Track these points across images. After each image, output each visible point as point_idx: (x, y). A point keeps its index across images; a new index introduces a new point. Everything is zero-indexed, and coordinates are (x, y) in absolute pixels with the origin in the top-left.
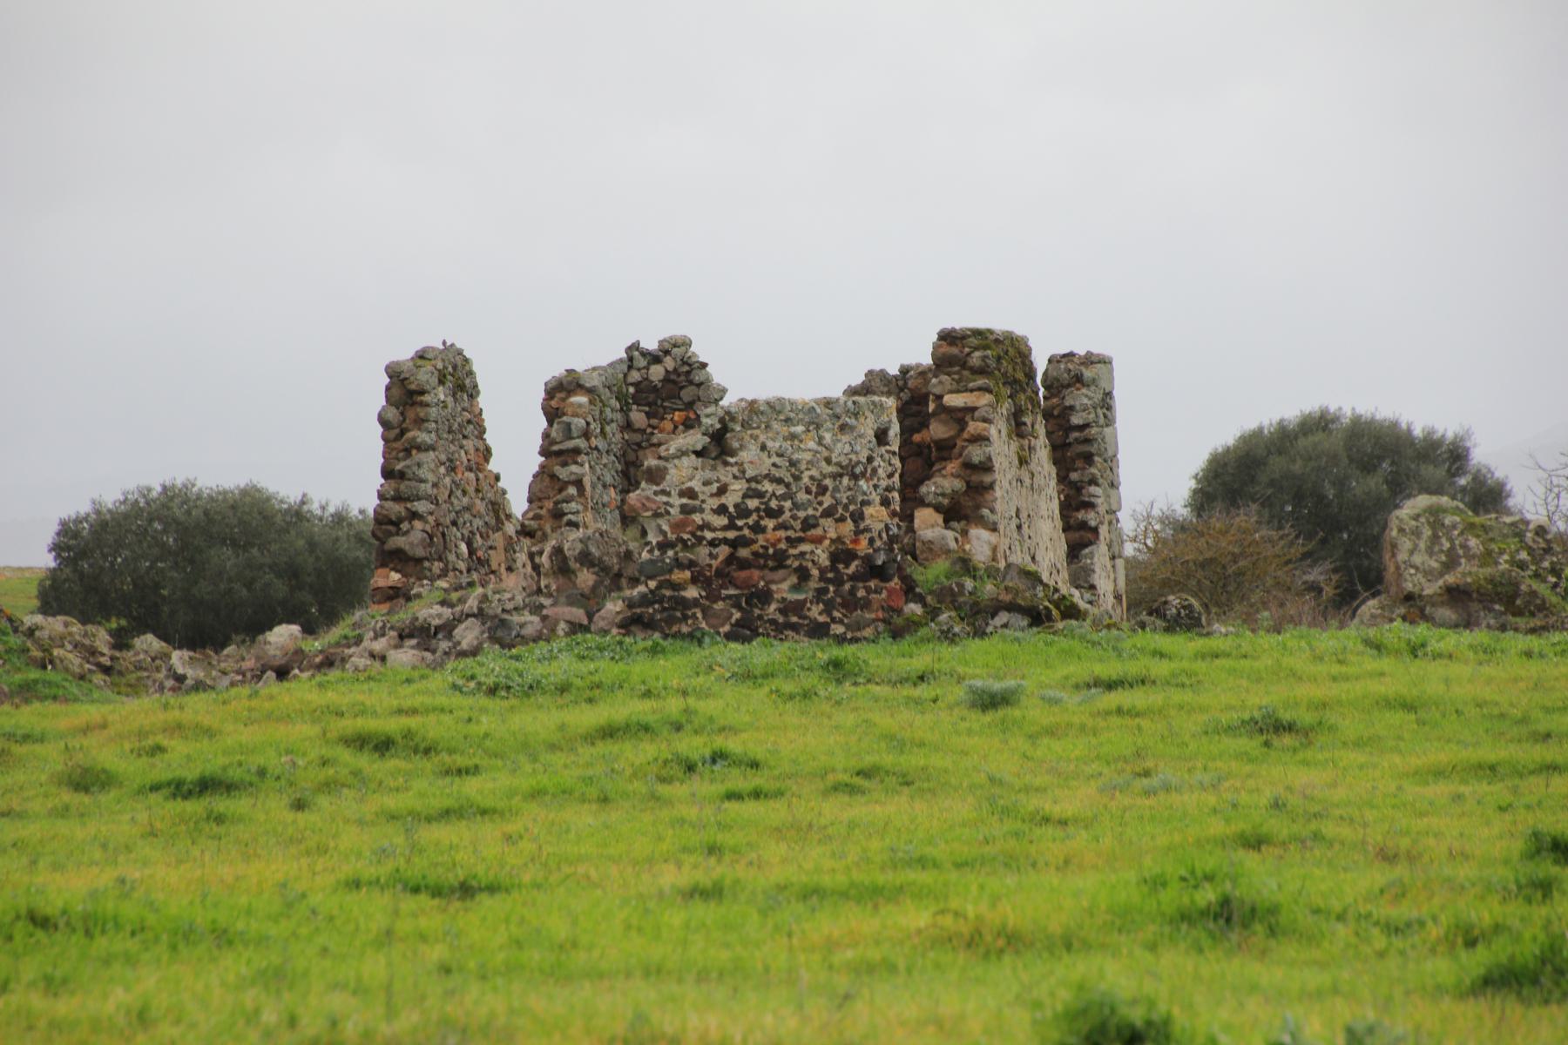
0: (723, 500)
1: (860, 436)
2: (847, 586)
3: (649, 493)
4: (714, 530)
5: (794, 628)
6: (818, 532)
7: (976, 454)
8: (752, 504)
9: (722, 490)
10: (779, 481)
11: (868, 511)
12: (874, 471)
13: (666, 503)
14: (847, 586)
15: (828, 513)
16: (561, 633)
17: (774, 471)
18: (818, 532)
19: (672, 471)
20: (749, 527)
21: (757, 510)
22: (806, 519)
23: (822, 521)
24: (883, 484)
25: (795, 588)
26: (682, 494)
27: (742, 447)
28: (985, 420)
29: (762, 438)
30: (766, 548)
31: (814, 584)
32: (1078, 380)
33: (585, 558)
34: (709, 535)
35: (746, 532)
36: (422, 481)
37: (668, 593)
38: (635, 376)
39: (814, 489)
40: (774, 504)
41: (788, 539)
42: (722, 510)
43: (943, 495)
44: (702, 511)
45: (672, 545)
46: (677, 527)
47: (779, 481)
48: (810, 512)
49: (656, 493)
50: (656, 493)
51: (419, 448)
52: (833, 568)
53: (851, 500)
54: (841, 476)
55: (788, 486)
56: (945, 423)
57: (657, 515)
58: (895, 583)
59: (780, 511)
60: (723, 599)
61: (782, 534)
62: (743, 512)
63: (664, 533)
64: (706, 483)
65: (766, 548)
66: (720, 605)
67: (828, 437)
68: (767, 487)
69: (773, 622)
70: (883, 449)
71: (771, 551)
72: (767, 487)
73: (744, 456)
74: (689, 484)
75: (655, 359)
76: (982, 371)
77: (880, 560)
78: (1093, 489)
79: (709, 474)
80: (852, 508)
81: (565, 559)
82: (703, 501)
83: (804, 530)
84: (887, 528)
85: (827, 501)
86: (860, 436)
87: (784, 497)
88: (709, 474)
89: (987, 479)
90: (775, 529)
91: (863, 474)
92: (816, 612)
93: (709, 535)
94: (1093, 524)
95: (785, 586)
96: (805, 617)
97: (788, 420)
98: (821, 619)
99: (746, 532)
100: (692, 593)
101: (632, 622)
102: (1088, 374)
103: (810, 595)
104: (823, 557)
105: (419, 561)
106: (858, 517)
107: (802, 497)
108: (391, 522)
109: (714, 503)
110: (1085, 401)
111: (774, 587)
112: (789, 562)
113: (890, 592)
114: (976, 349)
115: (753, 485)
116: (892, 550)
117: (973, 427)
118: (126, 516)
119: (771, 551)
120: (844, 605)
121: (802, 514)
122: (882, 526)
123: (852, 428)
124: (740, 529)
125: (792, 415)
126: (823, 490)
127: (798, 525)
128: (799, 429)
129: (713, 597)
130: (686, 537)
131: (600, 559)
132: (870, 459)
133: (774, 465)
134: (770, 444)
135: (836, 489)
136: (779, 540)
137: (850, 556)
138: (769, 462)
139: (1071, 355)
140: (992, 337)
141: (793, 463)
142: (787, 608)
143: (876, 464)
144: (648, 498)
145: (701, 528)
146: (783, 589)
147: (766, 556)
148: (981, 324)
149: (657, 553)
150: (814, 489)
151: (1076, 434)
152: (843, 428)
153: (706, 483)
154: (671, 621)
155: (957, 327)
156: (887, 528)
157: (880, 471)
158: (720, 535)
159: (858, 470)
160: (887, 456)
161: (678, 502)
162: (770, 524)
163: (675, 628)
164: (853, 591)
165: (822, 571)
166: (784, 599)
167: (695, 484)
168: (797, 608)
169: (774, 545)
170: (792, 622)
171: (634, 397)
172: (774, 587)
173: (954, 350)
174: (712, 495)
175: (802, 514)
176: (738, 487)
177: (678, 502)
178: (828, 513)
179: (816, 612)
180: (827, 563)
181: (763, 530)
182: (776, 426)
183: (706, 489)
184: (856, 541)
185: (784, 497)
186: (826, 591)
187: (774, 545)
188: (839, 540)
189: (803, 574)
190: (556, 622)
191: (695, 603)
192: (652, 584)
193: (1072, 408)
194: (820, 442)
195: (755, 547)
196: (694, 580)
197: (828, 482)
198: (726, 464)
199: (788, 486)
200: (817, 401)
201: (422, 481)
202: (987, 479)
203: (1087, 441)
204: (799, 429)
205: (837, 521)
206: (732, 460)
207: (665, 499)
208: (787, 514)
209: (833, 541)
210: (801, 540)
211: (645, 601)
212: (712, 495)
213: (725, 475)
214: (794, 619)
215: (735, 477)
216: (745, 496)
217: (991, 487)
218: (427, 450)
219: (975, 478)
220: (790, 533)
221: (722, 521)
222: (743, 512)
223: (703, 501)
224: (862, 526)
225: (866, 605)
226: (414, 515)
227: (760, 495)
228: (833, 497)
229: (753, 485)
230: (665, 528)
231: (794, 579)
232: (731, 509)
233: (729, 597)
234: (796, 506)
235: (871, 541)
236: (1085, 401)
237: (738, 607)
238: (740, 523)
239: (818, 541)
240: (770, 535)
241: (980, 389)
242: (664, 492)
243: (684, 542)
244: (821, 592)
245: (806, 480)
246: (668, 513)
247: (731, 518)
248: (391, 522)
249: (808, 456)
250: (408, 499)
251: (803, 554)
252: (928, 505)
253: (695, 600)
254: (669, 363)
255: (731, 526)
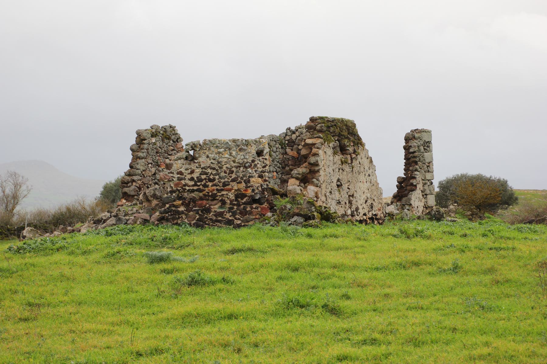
0: (193, 175)
1: (249, 153)
2: (242, 207)
3: (167, 173)
4: (189, 186)
5: (219, 221)
6: (230, 187)
7: (312, 160)
8: (203, 177)
9: (192, 172)
10: (214, 169)
11: (252, 180)
12: (256, 165)
13: (172, 177)
14: (242, 207)
15: (233, 180)
16: (138, 223)
17: (212, 165)
18: (230, 187)
19: (175, 165)
20: (202, 185)
21: (205, 179)
22: (224, 182)
23: (231, 183)
24: (260, 170)
25: (221, 207)
26: (178, 173)
27: (199, 157)
28: (318, 148)
29: (207, 153)
30: (208, 193)
31: (228, 206)
32: (414, 138)
33: (155, 196)
34: (187, 188)
35: (201, 187)
36: (138, 169)
37: (174, 209)
38: (288, 138)
39: (228, 172)
40: (212, 177)
41: (217, 190)
42: (192, 179)
43: (299, 174)
44: (185, 179)
45: (174, 192)
46: (176, 185)
47: (214, 169)
48: (226, 180)
49: (169, 173)
50: (169, 173)
51: (139, 158)
52: (236, 200)
53: (244, 176)
54: (240, 167)
55: (217, 170)
56: (306, 149)
57: (169, 181)
58: (266, 205)
59: (214, 180)
60: (193, 211)
61: (215, 188)
62: (200, 180)
63: (172, 187)
64: (187, 169)
65: (208, 193)
66: (191, 213)
67: (234, 153)
68: (209, 171)
69: (211, 219)
70: (261, 158)
71: (210, 194)
72: (209, 171)
73: (200, 159)
74: (180, 170)
75: (294, 133)
76: (320, 131)
77: (257, 197)
78: (416, 173)
79: (187, 166)
80: (244, 178)
81: (147, 197)
82: (185, 176)
83: (223, 186)
84: (261, 186)
85: (234, 176)
86: (249, 153)
87: (215, 175)
88: (187, 166)
89: (317, 168)
90: (212, 186)
91: (250, 166)
92: (228, 216)
93: (187, 188)
94: (415, 184)
95: (217, 206)
96: (224, 218)
97: (217, 147)
98: (230, 218)
99: (201, 187)
100: (182, 209)
101: (161, 220)
102: (417, 135)
103: (227, 210)
104: (232, 196)
105: (133, 196)
106: (247, 182)
107: (223, 174)
108: (125, 183)
109: (189, 176)
110: (415, 144)
111: (212, 207)
112: (217, 198)
113: (262, 209)
114: (320, 123)
115: (204, 170)
116: (264, 194)
117: (314, 150)
118: (452, 180)
119: (210, 194)
120: (241, 213)
121: (223, 181)
122: (260, 185)
123: (245, 150)
124: (199, 186)
125: (219, 145)
126: (232, 172)
127: (221, 185)
128: (222, 150)
129: (189, 210)
130: (179, 189)
131: (160, 197)
132: (253, 161)
133: (211, 163)
134: (210, 155)
135: (237, 172)
136: (214, 190)
137: (243, 196)
138: (210, 162)
139: (417, 130)
140: (326, 119)
141: (219, 163)
142: (218, 214)
143: (256, 163)
144: (166, 175)
145: (185, 185)
146: (216, 207)
147: (209, 196)
148: (321, 115)
149: (169, 194)
150: (228, 172)
151: (411, 155)
152: (241, 150)
153: (187, 169)
154: (174, 219)
155: (315, 116)
156: (261, 186)
157: (258, 165)
158: (191, 188)
159: (247, 165)
160: (262, 160)
161: (176, 176)
162: (210, 184)
163: (175, 222)
164: (245, 208)
165: (231, 201)
166: (215, 211)
167: (183, 170)
168: (221, 214)
169: (211, 192)
170: (219, 221)
171: (287, 144)
172: (212, 207)
173: (312, 124)
174: (189, 174)
175: (223, 181)
176: (198, 171)
177: (176, 176)
178: (233, 180)
179: (228, 216)
180: (234, 198)
181: (208, 186)
182: (212, 149)
183: (186, 171)
184: (246, 190)
185: (215, 175)
186: (233, 208)
187: (211, 192)
188: (239, 190)
189: (223, 203)
190: (138, 218)
191: (182, 212)
192: (167, 206)
193: (411, 146)
194: (231, 154)
195: (204, 192)
196: (182, 204)
197: (234, 169)
198: (194, 162)
199: (217, 170)
200: (230, 141)
201: (138, 169)
202: (317, 168)
203: (415, 157)
204: (222, 150)
205: (238, 183)
206: (196, 161)
207: (172, 175)
208: (217, 181)
209: (236, 190)
210: (222, 190)
211: (166, 212)
212: (189, 174)
213: (193, 166)
214: (220, 218)
215: (197, 167)
216: (201, 174)
217: (318, 171)
218: (142, 159)
219: (313, 168)
220: (218, 187)
221: (192, 183)
222: (200, 180)
223: (185, 176)
224: (249, 185)
225: (251, 213)
226: (133, 181)
227: (206, 174)
228: (236, 175)
229: (204, 170)
230: (172, 185)
231: (220, 204)
232: (195, 179)
233: (195, 210)
234: (220, 178)
235: (253, 191)
236: (415, 144)
237: (198, 213)
238: (199, 184)
239: (230, 190)
240: (210, 188)
241: (317, 137)
242: (171, 173)
243: (179, 190)
244: (230, 209)
245: (224, 168)
246: (173, 180)
247: (196, 182)
248: (125, 183)
249: (225, 160)
250: (133, 175)
251: (223, 195)
252: (293, 178)
253: (182, 211)
254: (297, 134)
255: (195, 185)
